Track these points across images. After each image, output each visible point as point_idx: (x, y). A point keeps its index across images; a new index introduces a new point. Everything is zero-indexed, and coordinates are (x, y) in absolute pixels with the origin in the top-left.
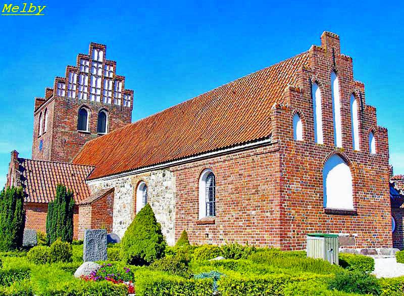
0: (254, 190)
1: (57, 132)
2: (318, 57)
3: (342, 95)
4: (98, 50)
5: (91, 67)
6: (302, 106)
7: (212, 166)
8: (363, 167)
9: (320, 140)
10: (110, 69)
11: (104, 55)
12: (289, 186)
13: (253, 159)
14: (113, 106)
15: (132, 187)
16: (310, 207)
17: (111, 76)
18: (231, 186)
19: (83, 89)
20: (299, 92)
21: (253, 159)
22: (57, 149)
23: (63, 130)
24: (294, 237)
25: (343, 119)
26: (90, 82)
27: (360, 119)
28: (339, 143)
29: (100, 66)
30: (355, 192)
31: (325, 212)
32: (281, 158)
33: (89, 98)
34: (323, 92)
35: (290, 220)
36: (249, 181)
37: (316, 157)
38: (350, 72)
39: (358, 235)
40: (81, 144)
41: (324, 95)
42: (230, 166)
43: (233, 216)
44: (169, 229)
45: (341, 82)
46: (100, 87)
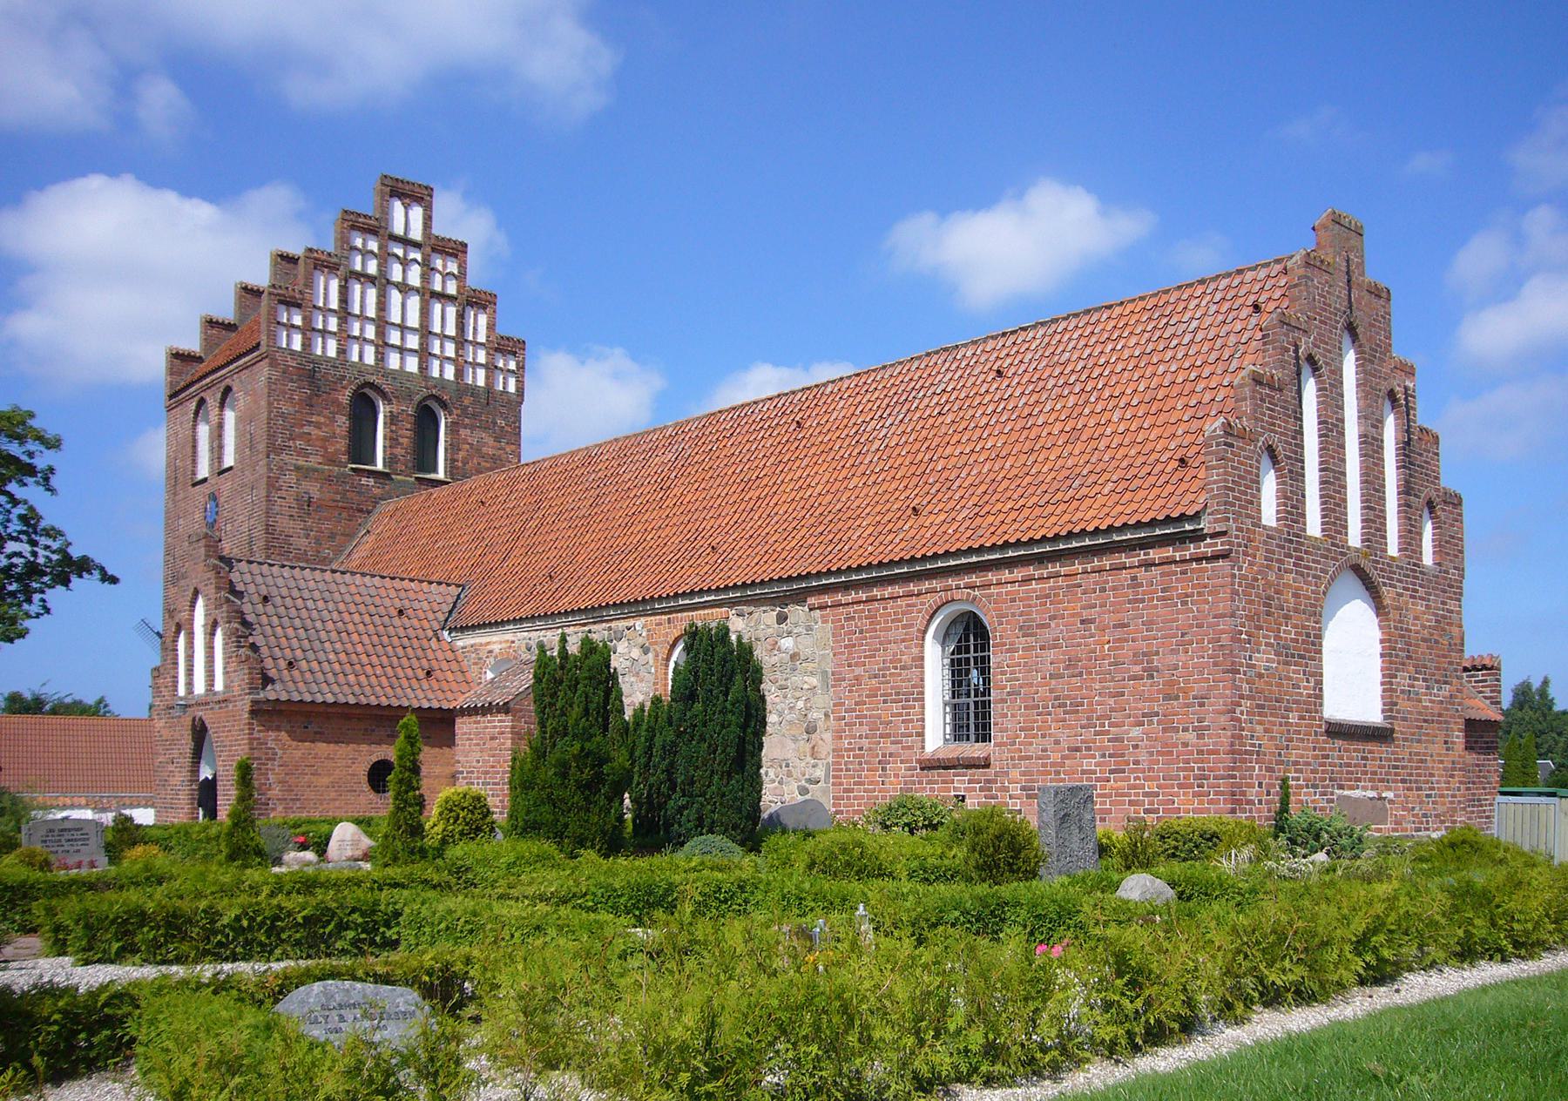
0: (1138, 668)
1: (281, 468)
2: (1314, 286)
3: (1366, 398)
4: (407, 201)
5: (384, 257)
6: (1280, 426)
7: (977, 593)
8: (1407, 603)
9: (1314, 525)
10: (445, 266)
11: (428, 220)
12: (1250, 657)
13: (1134, 578)
14: (461, 387)
15: (650, 655)
16: (1293, 718)
17: (452, 289)
18: (1051, 654)
19: (362, 330)
20: (1272, 388)
21: (1134, 578)
22: (284, 524)
23: (301, 462)
24: (1260, 802)
25: (1367, 468)
26: (382, 306)
27: (1404, 467)
28: (1354, 537)
29: (416, 255)
30: (1389, 676)
31: (1327, 731)
32: (1234, 576)
33: (381, 357)
34: (1326, 389)
35: (1250, 753)
36: (1119, 640)
37: (1308, 575)
38: (1385, 331)
39: (1395, 796)
40: (361, 511)
41: (1326, 396)
42: (1048, 596)
43: (1057, 742)
44: (810, 781)
45: (1365, 359)
46: (416, 325)
